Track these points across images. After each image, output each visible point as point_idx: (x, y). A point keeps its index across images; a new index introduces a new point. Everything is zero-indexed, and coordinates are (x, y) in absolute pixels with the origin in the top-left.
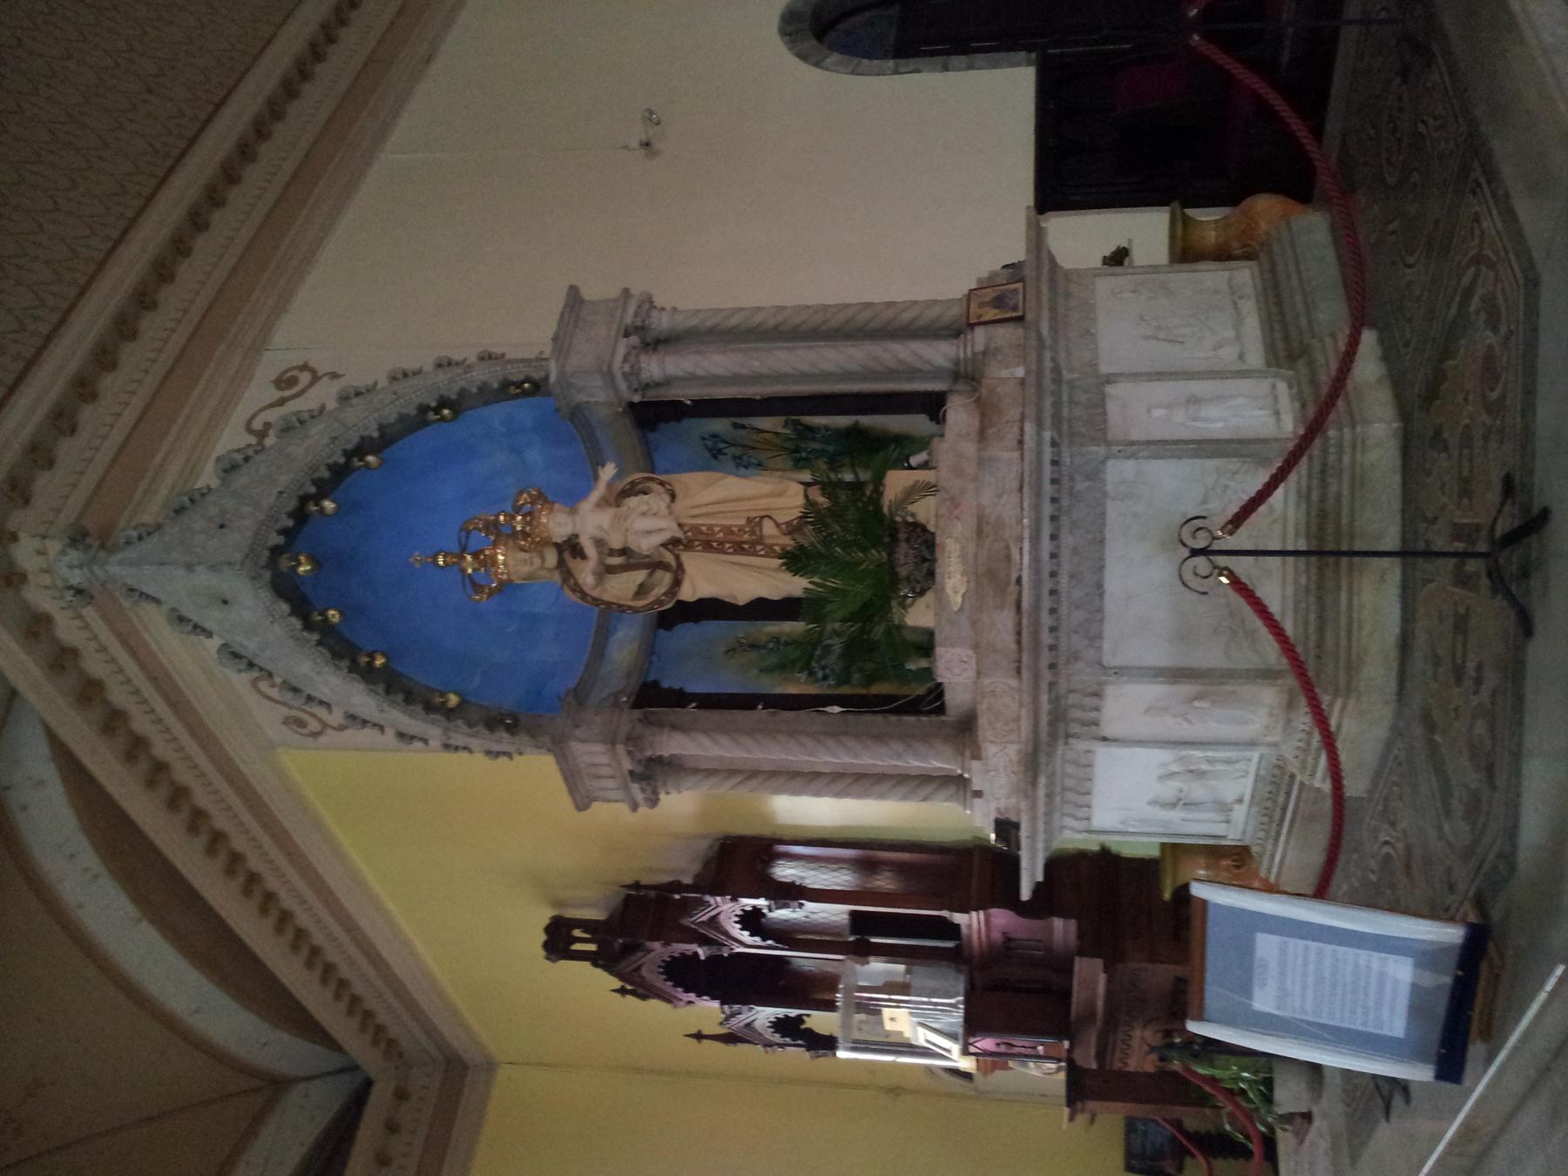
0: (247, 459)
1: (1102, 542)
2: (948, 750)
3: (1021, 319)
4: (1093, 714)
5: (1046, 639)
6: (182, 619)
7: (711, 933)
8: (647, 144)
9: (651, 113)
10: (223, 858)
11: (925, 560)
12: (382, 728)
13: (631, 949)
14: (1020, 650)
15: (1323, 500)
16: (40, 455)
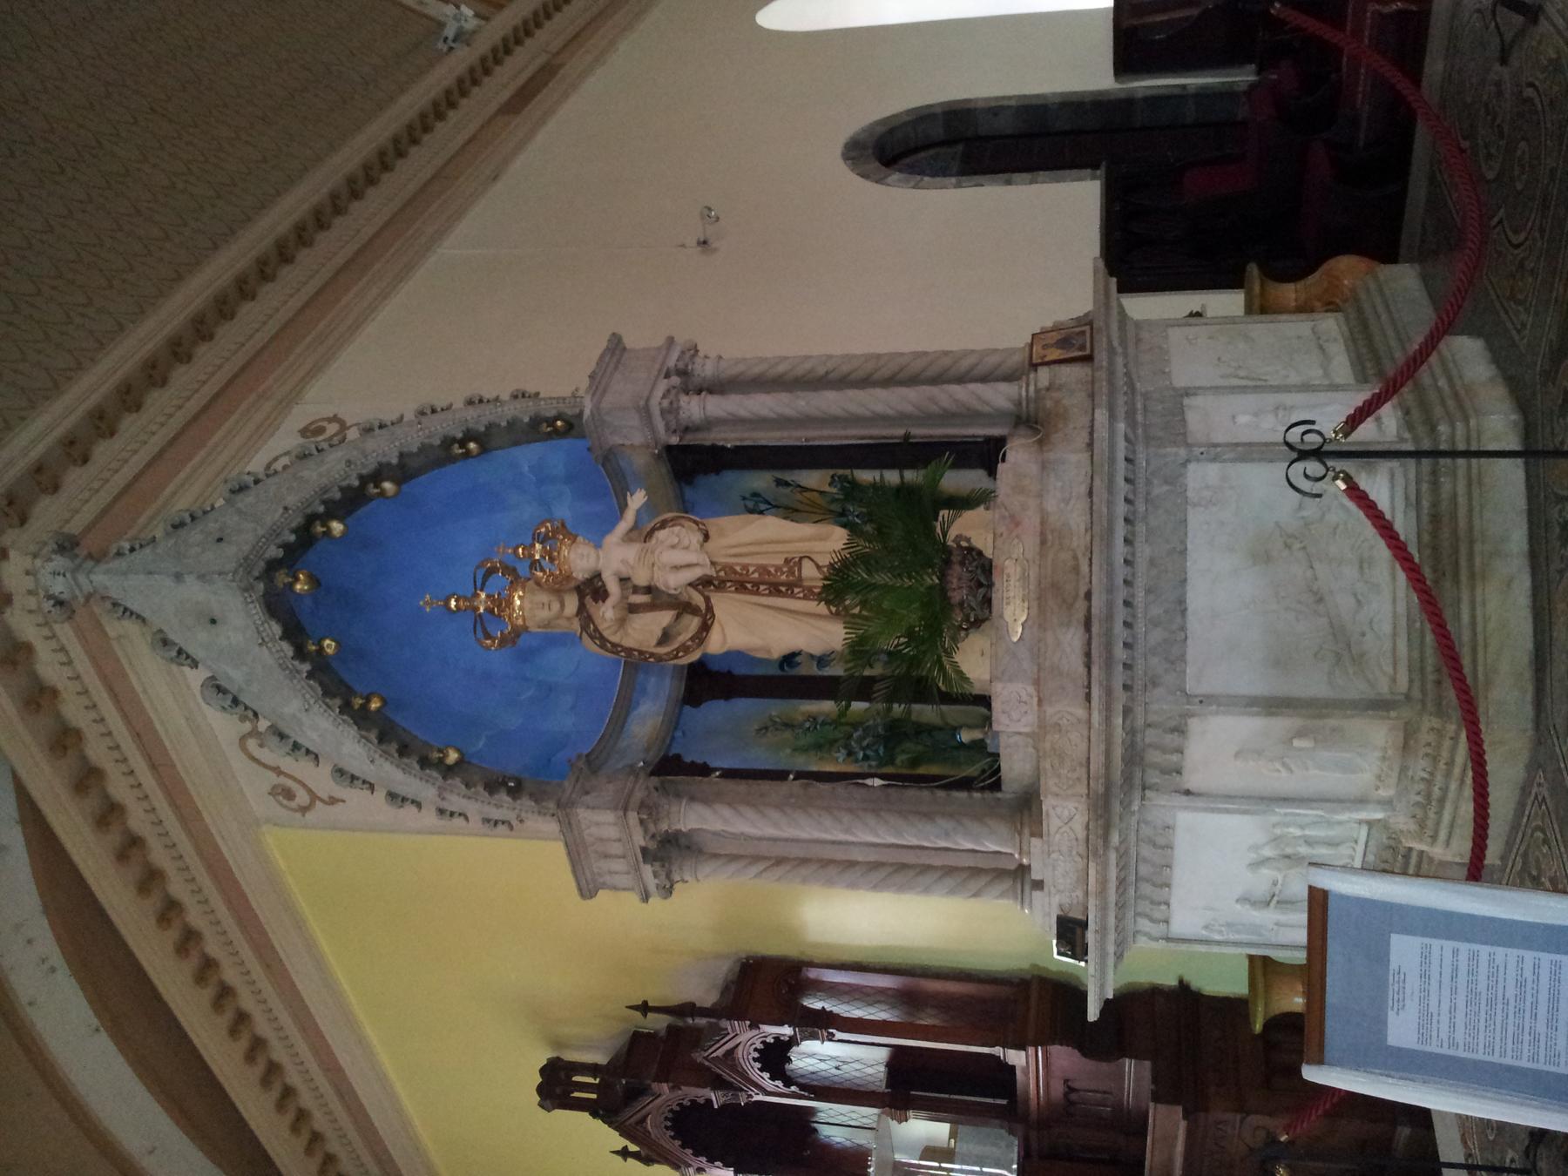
0: (257, 482)
1: (1183, 552)
2: (1003, 829)
3: (1088, 359)
4: (1175, 758)
5: (1120, 653)
6: (166, 642)
7: (724, 1075)
8: (705, 242)
9: (710, 209)
10: (194, 961)
11: (980, 585)
12: (372, 787)
13: (635, 1093)
14: (1088, 667)
15: (1435, 505)
16: (44, 477)
